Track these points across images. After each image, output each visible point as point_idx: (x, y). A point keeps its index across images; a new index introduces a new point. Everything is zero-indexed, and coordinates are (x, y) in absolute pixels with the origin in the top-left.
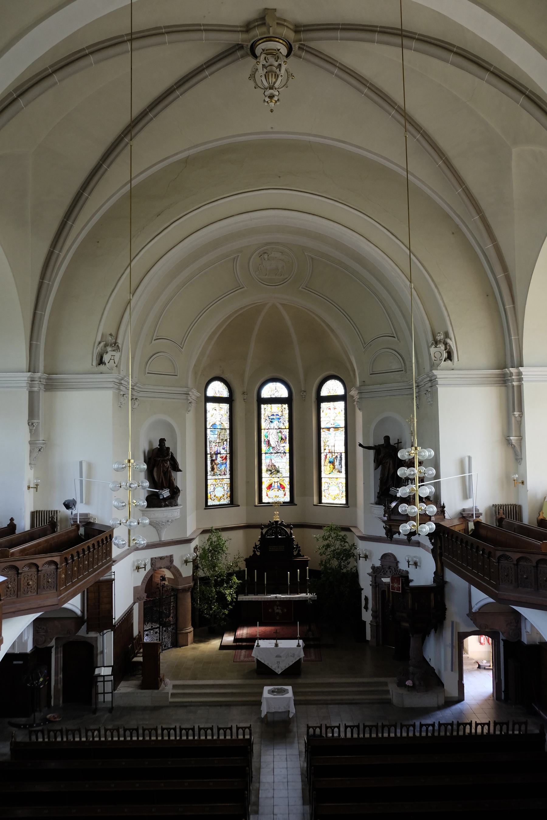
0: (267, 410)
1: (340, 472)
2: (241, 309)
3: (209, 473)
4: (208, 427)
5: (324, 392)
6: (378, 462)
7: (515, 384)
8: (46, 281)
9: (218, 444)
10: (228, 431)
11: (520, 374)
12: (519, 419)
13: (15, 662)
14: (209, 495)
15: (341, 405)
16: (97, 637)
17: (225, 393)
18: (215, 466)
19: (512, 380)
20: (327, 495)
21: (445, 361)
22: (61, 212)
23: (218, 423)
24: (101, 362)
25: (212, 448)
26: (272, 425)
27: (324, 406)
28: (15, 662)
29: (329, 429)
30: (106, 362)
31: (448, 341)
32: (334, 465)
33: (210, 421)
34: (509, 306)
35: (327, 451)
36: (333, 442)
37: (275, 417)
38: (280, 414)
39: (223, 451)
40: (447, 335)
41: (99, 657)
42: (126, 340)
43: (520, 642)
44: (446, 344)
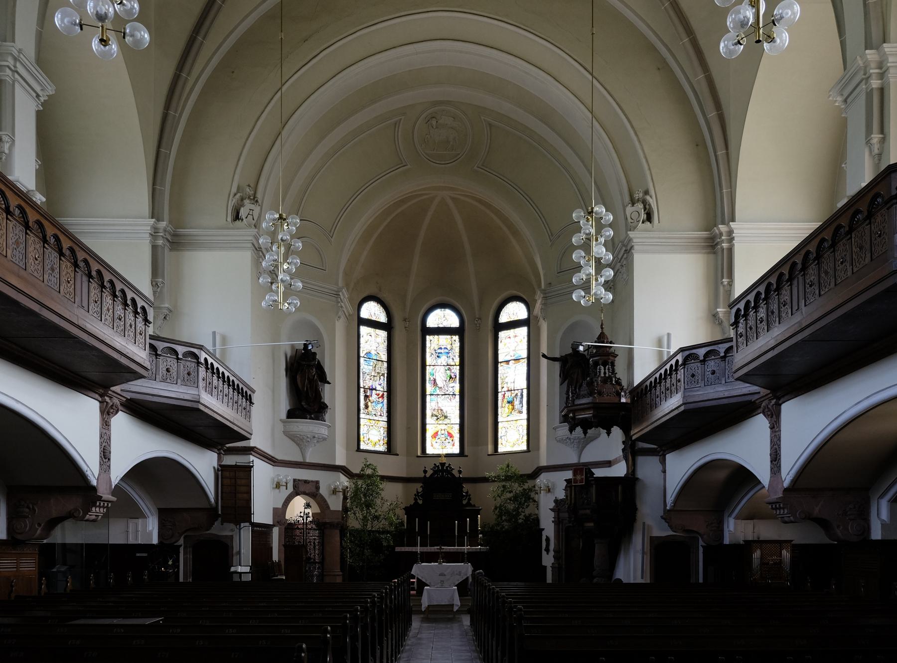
0: (433, 342)
1: (521, 412)
2: (403, 201)
3: (362, 411)
4: (362, 355)
5: (504, 318)
6: (565, 375)
7: (725, 245)
8: (171, 112)
9: (373, 376)
10: (385, 365)
11: (730, 232)
12: (727, 288)
13: (138, 555)
14: (362, 437)
15: (523, 331)
16: (232, 536)
17: (382, 318)
18: (369, 404)
19: (722, 241)
20: (504, 443)
21: (643, 222)
22: (189, 23)
23: (373, 352)
24: (237, 217)
25: (365, 382)
26: (439, 361)
27: (502, 334)
28: (138, 555)
29: (507, 362)
30: (244, 217)
31: (648, 198)
32: (513, 405)
33: (364, 348)
34: (721, 152)
35: (505, 389)
36: (513, 377)
37: (442, 351)
38: (449, 347)
39: (379, 388)
40: (647, 192)
41: (234, 558)
42: (266, 192)
43: (722, 543)
44: (644, 202)
